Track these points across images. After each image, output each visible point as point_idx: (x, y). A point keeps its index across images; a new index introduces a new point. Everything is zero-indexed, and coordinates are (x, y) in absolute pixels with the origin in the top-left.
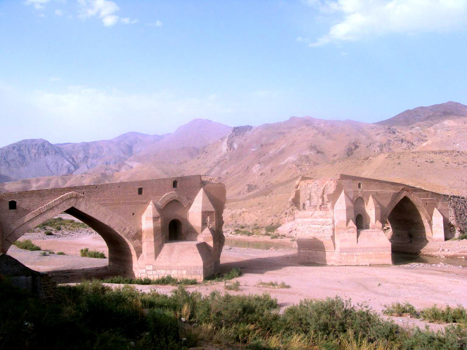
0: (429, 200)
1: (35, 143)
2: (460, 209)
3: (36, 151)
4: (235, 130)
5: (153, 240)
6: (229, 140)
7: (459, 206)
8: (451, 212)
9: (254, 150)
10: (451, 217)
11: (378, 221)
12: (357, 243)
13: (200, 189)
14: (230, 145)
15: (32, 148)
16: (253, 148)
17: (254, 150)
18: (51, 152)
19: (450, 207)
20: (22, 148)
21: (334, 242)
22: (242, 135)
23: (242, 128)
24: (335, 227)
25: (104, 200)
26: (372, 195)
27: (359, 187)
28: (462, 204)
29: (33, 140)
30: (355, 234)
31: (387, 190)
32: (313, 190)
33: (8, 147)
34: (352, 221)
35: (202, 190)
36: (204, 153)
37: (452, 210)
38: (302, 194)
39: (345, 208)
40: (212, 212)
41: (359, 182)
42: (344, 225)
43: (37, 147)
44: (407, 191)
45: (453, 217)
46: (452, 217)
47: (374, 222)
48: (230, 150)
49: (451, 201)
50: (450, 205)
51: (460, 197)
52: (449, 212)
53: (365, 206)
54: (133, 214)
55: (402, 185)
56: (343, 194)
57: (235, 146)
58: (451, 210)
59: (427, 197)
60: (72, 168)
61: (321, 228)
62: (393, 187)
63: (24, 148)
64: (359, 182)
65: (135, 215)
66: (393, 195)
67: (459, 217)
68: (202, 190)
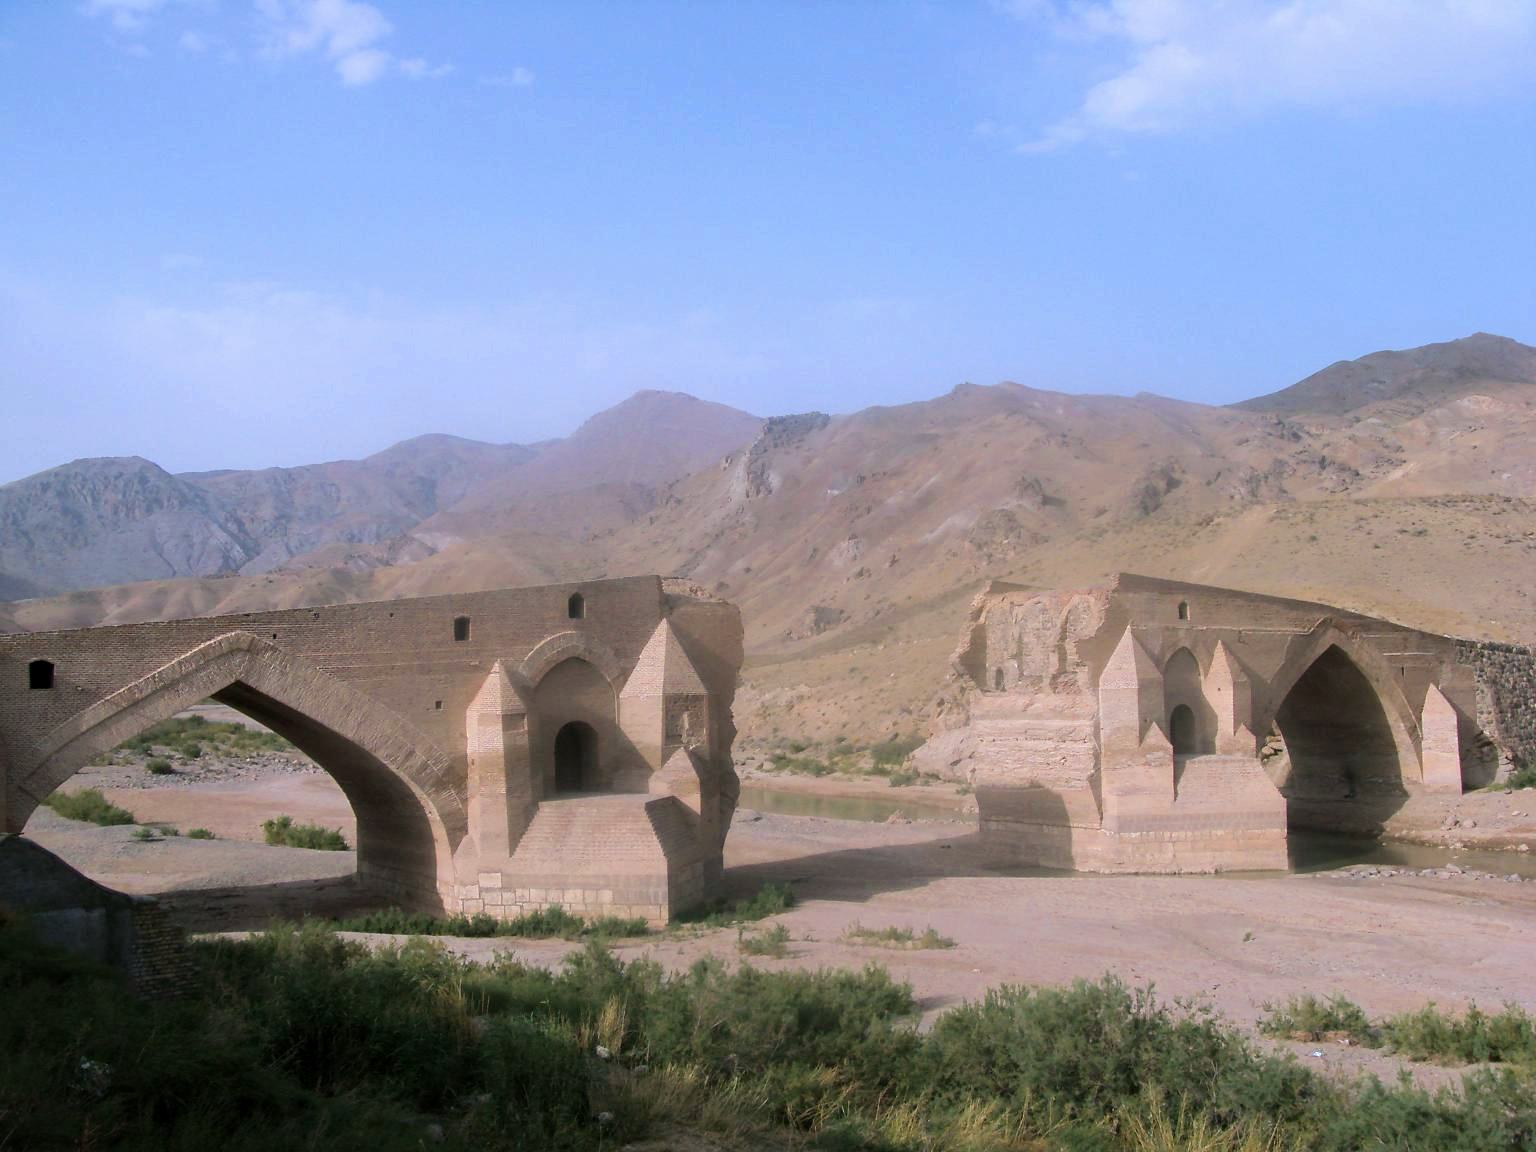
0: (1410, 657)
1: (114, 471)
2: (1514, 688)
3: (120, 497)
4: (774, 427)
5: (503, 791)
6: (752, 462)
7: (1511, 679)
8: (1483, 698)
9: (836, 492)
10: (1482, 713)
11: (1243, 727)
12: (1175, 799)
13: (657, 624)
14: (757, 478)
15: (106, 487)
16: (832, 488)
17: (836, 492)
18: (169, 501)
19: (1479, 681)
20: (73, 487)
21: (1100, 796)
22: (795, 445)
23: (796, 422)
24: (1103, 747)
25: (342, 658)
26: (1223, 643)
27: (1182, 615)
28: (1519, 670)
29: (109, 462)
30: (1169, 770)
31: (1271, 625)
32: (1032, 625)
33: (28, 483)
34: (1156, 727)
35: (663, 626)
36: (672, 503)
37: (1486, 690)
38: (992, 640)
39: (1135, 686)
40: (697, 698)
41: (1180, 598)
42: (1132, 742)
43: (121, 483)
44: (1340, 628)
45: (1490, 713)
46: (1485, 715)
47: (1232, 730)
48: (758, 492)
49: (1482, 661)
50: (1481, 676)
51: (1514, 650)
52: (1478, 698)
53: (1202, 678)
54: (438, 704)
55: (1322, 608)
56: (1127, 638)
57: (774, 480)
58: (1482, 692)
59: (1405, 648)
60: (237, 552)
61: (1055, 749)
62: (1293, 614)
63: (79, 486)
64: (1180, 598)
65: (445, 708)
66: (1292, 641)
67: (1509, 715)
68: (663, 626)
